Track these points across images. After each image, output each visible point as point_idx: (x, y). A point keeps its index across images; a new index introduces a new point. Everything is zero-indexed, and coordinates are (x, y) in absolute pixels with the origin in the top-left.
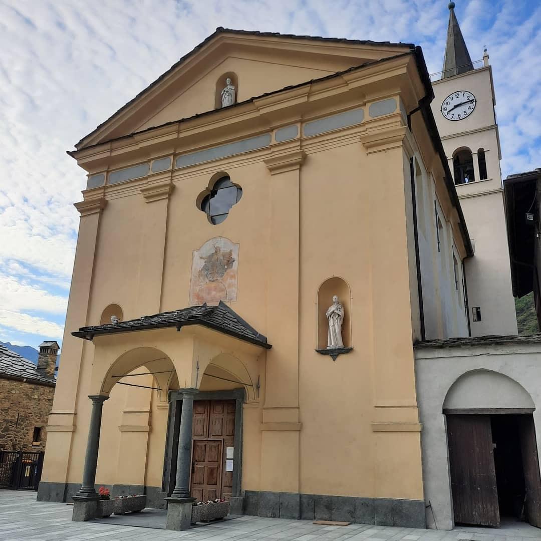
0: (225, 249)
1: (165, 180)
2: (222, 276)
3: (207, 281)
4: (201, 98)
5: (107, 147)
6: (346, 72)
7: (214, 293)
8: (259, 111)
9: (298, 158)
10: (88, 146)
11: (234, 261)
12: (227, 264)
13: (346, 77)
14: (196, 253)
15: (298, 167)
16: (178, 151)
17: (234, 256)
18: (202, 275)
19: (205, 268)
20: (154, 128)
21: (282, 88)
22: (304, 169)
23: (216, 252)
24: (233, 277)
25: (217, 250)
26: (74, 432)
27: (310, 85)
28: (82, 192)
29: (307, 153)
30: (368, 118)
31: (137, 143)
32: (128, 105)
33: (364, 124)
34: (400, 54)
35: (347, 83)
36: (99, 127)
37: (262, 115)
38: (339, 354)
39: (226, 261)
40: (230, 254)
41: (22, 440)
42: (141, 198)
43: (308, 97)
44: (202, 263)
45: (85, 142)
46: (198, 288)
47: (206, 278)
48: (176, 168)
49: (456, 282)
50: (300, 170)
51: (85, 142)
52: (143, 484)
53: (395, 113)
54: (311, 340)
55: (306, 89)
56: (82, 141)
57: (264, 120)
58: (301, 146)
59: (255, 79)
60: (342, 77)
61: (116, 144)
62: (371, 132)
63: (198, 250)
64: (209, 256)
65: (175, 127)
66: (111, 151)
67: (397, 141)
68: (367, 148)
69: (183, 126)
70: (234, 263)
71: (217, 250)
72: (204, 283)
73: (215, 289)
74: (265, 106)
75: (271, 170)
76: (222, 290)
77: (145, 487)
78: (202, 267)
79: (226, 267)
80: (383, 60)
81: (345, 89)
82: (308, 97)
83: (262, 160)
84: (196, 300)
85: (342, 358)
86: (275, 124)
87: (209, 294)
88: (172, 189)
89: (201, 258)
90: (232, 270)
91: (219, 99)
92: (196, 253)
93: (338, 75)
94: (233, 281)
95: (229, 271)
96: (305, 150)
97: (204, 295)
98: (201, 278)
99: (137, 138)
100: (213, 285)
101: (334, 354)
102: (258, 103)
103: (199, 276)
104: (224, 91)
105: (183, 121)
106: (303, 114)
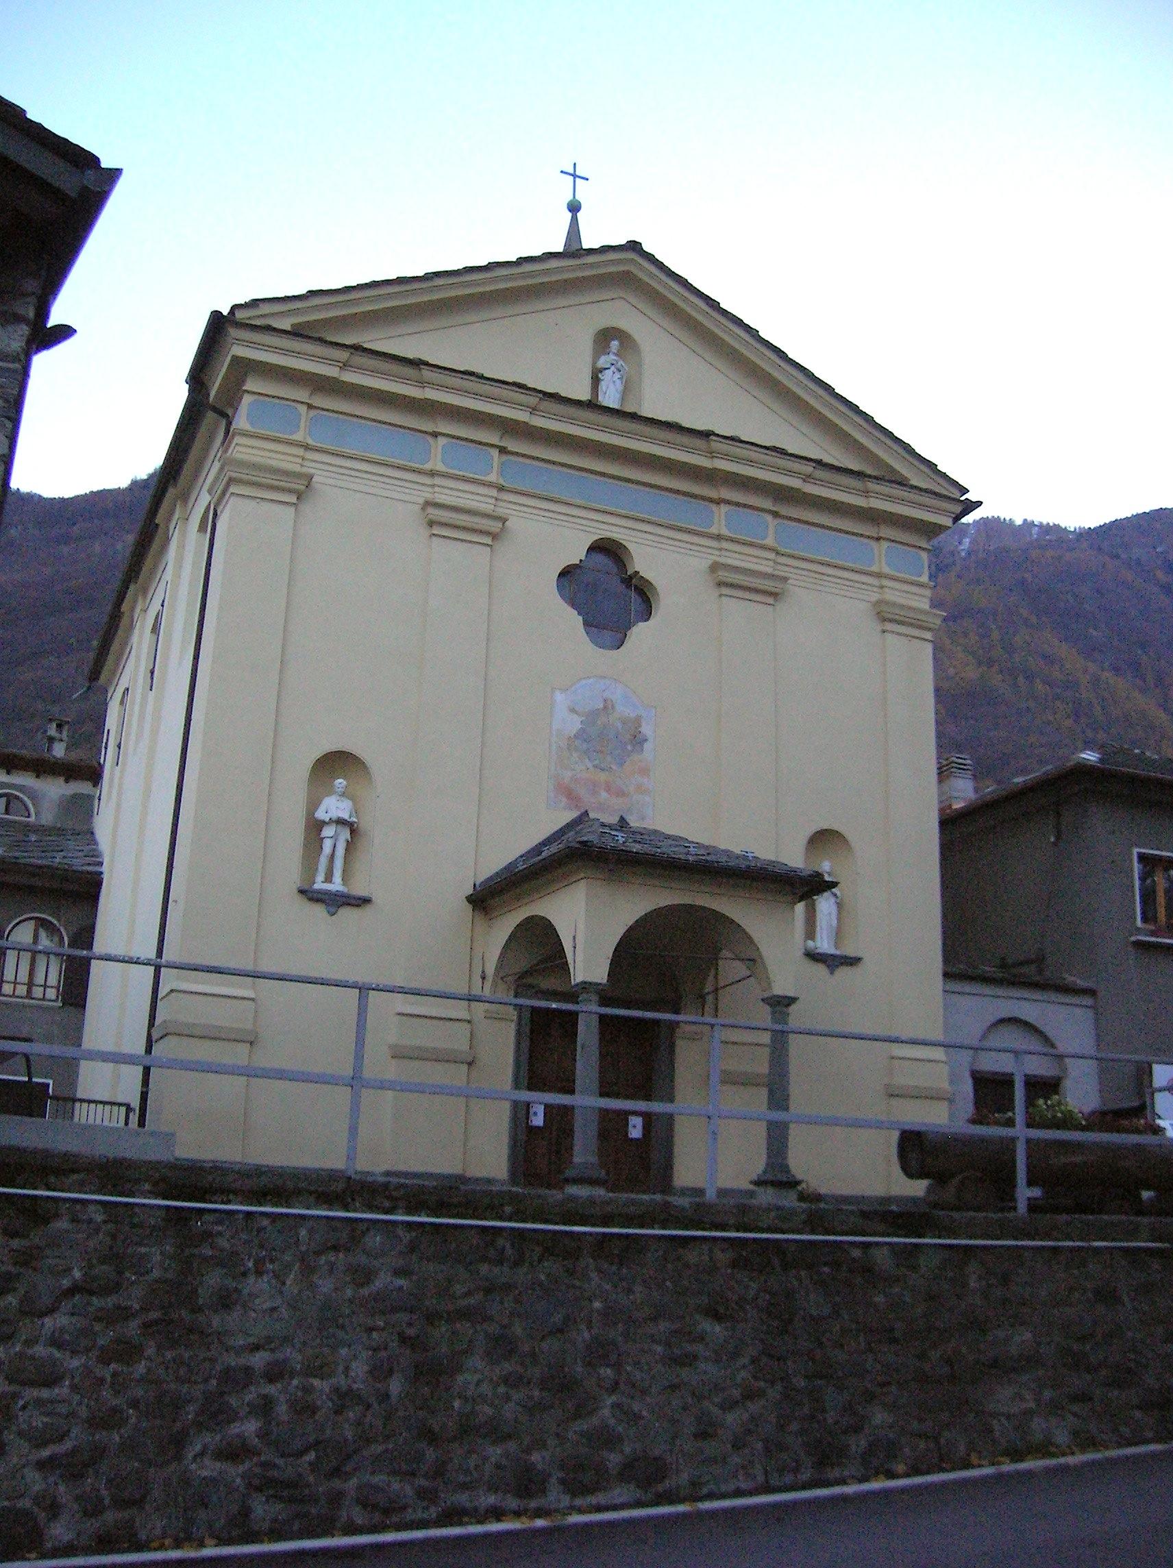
3: (590, 765)
6: (876, 478)
7: (604, 795)
13: (871, 486)
14: (559, 697)
17: (646, 729)
19: (581, 735)
21: (768, 445)
22: (306, 508)
23: (605, 708)
24: (644, 771)
25: (608, 706)
32: (400, 281)
34: (946, 493)
36: (312, 294)
38: (842, 964)
40: (638, 721)
41: (684, 1373)
44: (574, 724)
46: (568, 775)
49: (152, 673)
52: (79, 1095)
55: (808, 469)
59: (676, 384)
62: (890, 596)
63: (564, 690)
65: (533, 400)
67: (930, 629)
68: (884, 620)
69: (548, 405)
70: (646, 745)
71: (608, 706)
73: (608, 789)
74: (726, 456)
76: (621, 793)
77: (74, 1100)
79: (629, 748)
80: (926, 491)
81: (860, 502)
84: (564, 800)
89: (573, 710)
92: (559, 697)
93: (859, 475)
97: (582, 792)
98: (575, 755)
100: (603, 777)
102: (716, 445)
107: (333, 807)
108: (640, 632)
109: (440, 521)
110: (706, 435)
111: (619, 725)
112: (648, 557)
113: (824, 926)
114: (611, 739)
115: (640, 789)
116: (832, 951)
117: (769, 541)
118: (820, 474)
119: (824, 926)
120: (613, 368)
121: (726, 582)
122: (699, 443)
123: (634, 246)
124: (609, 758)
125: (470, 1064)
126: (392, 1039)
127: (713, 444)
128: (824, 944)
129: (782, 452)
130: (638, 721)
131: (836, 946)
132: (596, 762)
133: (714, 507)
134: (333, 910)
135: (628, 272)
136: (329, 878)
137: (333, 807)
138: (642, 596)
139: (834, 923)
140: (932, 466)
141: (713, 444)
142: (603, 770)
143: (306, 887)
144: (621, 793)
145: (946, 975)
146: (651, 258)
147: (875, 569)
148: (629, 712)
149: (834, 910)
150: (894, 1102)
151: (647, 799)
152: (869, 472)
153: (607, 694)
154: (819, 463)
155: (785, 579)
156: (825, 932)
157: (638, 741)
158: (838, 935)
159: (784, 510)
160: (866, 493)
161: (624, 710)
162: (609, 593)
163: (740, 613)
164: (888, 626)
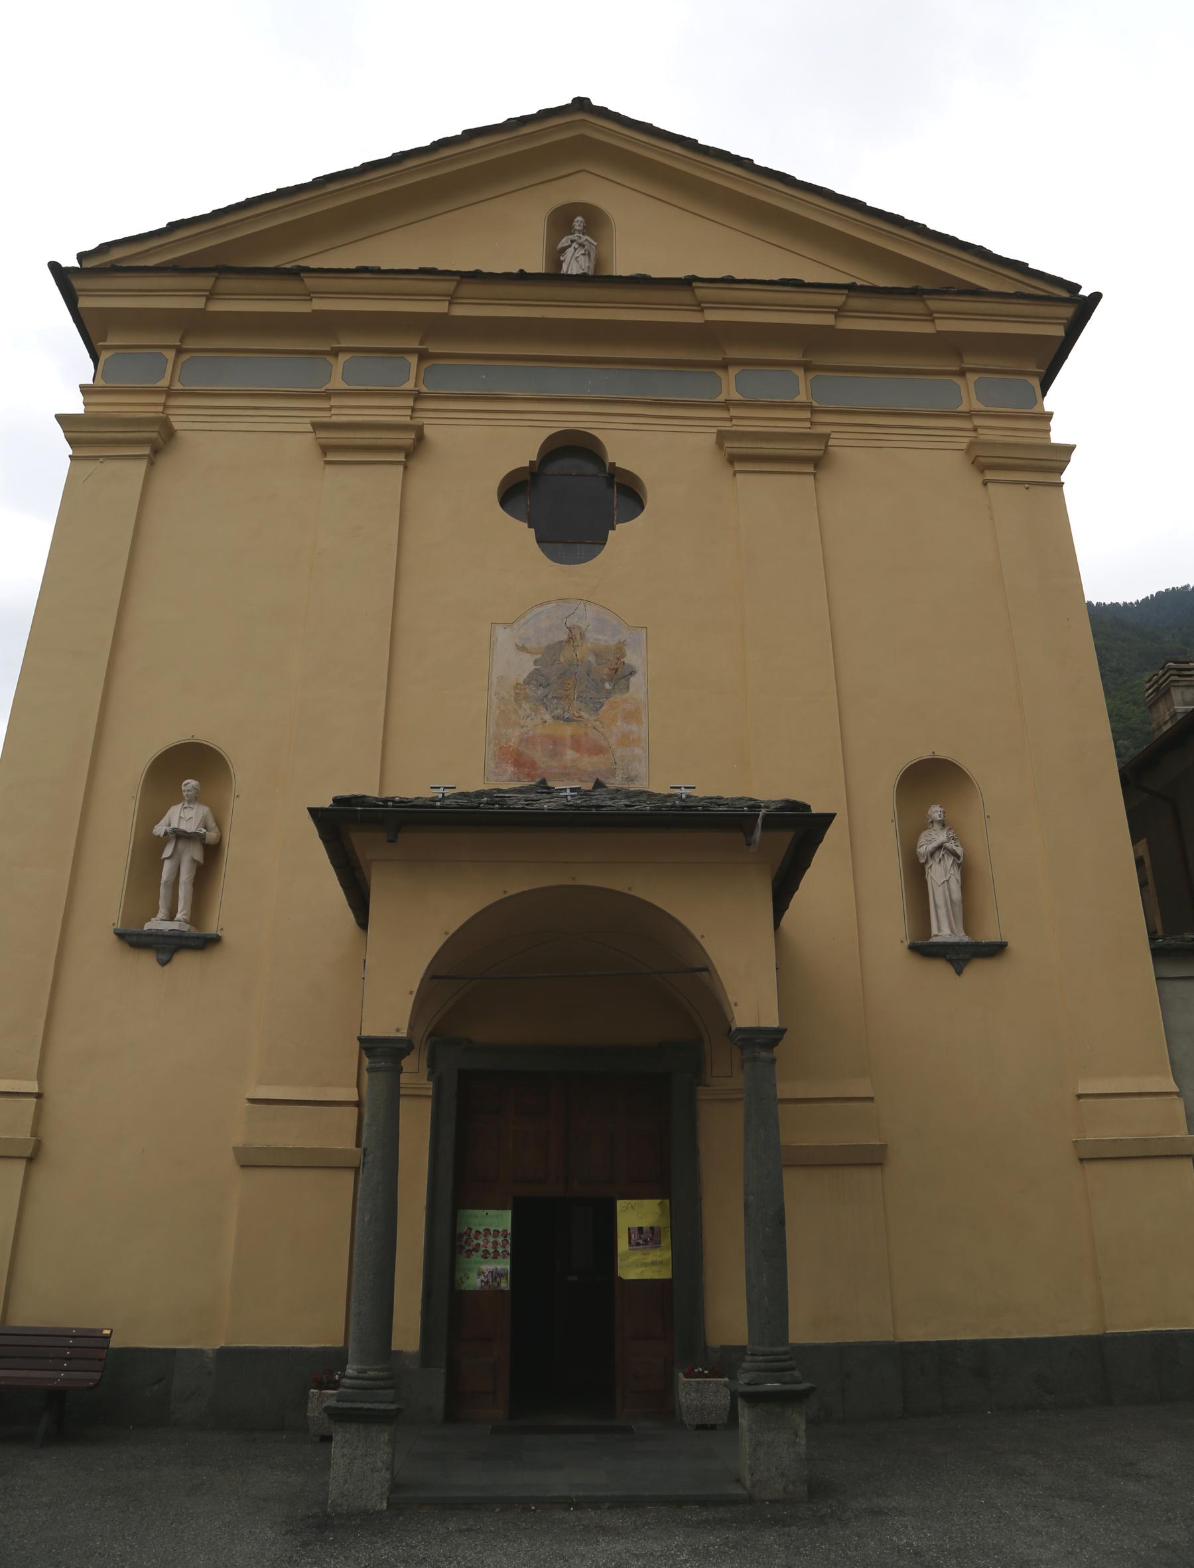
0: (601, 637)
1: (395, 412)
2: (597, 710)
3: (547, 717)
4: (507, 237)
5: (206, 282)
7: (570, 754)
8: (702, 310)
9: (408, 438)
10: (124, 265)
11: (632, 673)
12: (611, 680)
13: (934, 304)
14: (502, 634)
15: (146, 451)
16: (433, 349)
18: (526, 698)
19: (537, 678)
20: (377, 271)
21: (776, 278)
22: (166, 463)
23: (571, 639)
25: (574, 636)
26: (30, 1160)
27: (846, 292)
28: (81, 387)
29: (176, 426)
30: (337, 383)
31: (309, 296)
32: (282, 193)
33: (328, 395)
35: (931, 315)
36: (173, 226)
37: (939, 333)
39: (606, 670)
40: (620, 649)
42: (307, 442)
43: (208, 299)
44: (527, 665)
45: (116, 254)
47: (543, 710)
48: (178, 386)
50: (152, 464)
51: (116, 254)
53: (403, 387)
54: (892, 929)
55: (838, 299)
56: (105, 248)
57: (709, 335)
58: (165, 406)
59: (651, 239)
60: (923, 301)
61: (229, 283)
62: (986, 435)
63: (507, 625)
64: (548, 647)
65: (448, 286)
66: (211, 295)
68: (982, 468)
69: (468, 289)
70: (633, 679)
71: (574, 636)
72: (536, 722)
73: (577, 745)
75: (325, 449)
78: (525, 675)
79: (607, 686)
81: (926, 328)
82: (208, 299)
83: (308, 420)
84: (511, 769)
85: (185, 962)
86: (733, 353)
87: (555, 754)
88: (413, 448)
89: (522, 649)
90: (625, 696)
91: (555, 256)
92: (502, 634)
94: (634, 728)
95: (617, 698)
96: (172, 419)
97: (539, 756)
98: (526, 706)
99: (311, 282)
100: (567, 730)
101: (166, 947)
102: (702, 292)
103: (516, 700)
104: (572, 241)
105: (476, 276)
106: (814, 347)
107: (184, 816)
108: (622, 535)
109: (338, 446)
110: (688, 282)
111: (592, 658)
112: (628, 443)
113: (940, 901)
114: (580, 677)
115: (626, 740)
116: (961, 937)
117: (802, 398)
118: (857, 303)
119: (940, 901)
120: (575, 245)
121: (740, 455)
122: (683, 296)
123: (581, 104)
124: (576, 704)
125: (30, 1160)
126: (238, 1140)
127: (697, 291)
128: (944, 930)
129: (798, 284)
130: (620, 649)
131: (967, 932)
132: (559, 711)
133: (720, 373)
134: (164, 957)
135: (583, 137)
136: (171, 917)
137: (184, 816)
138: (628, 494)
139: (957, 895)
140: (1020, 267)
141: (697, 291)
142: (568, 720)
143: (133, 929)
144: (598, 750)
145: (1158, 953)
146: (603, 112)
147: (963, 408)
148: (607, 640)
149: (955, 876)
150: (1092, 1169)
151: (637, 751)
152: (926, 286)
153: (572, 621)
154: (851, 287)
155: (827, 437)
156: (942, 912)
157: (621, 675)
158: (968, 909)
159: (818, 360)
160: (930, 316)
161: (599, 638)
162: (570, 498)
163: (769, 494)
164: (989, 475)
